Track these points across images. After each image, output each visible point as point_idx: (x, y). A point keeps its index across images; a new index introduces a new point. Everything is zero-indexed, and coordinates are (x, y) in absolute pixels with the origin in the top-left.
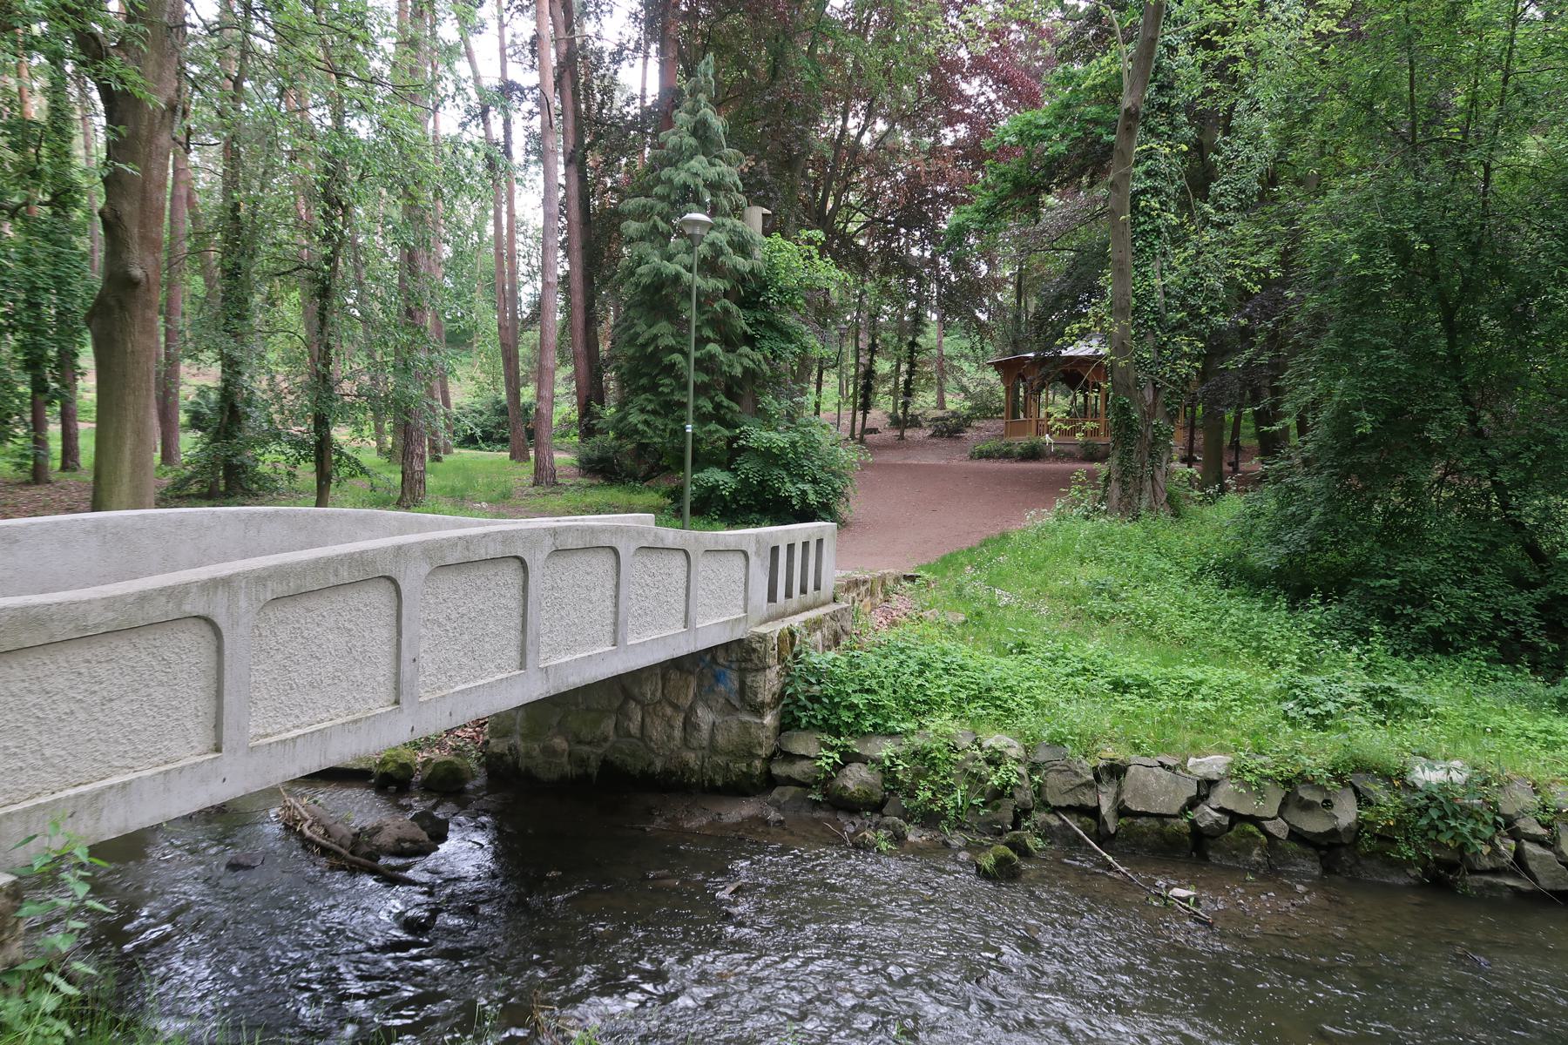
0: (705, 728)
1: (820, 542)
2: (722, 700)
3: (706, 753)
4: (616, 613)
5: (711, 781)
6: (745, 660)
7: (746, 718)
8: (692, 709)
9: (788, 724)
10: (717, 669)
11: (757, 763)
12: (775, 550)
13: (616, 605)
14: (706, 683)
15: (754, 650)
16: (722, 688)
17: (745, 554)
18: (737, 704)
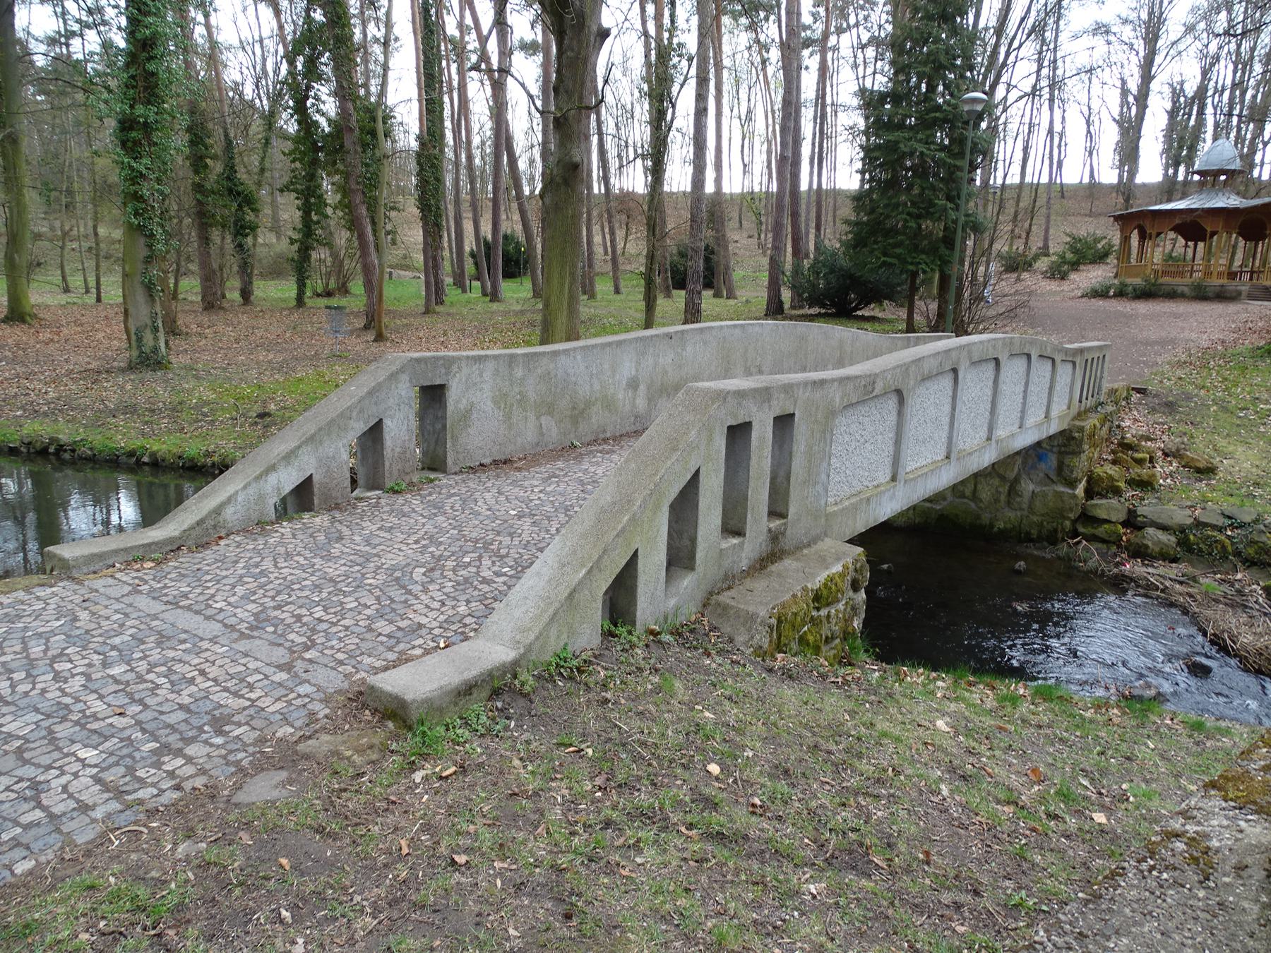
0: (1027, 495)
1: (784, 422)
2: (1041, 475)
3: (1026, 513)
4: (1024, 404)
5: (1028, 534)
6: (1065, 445)
7: (1061, 489)
8: (1017, 480)
9: (1089, 494)
10: (1041, 451)
11: (1068, 523)
12: (738, 433)
13: (1025, 398)
14: (1030, 462)
15: (1074, 438)
16: (1043, 466)
17: (1053, 360)
18: (1054, 478)
